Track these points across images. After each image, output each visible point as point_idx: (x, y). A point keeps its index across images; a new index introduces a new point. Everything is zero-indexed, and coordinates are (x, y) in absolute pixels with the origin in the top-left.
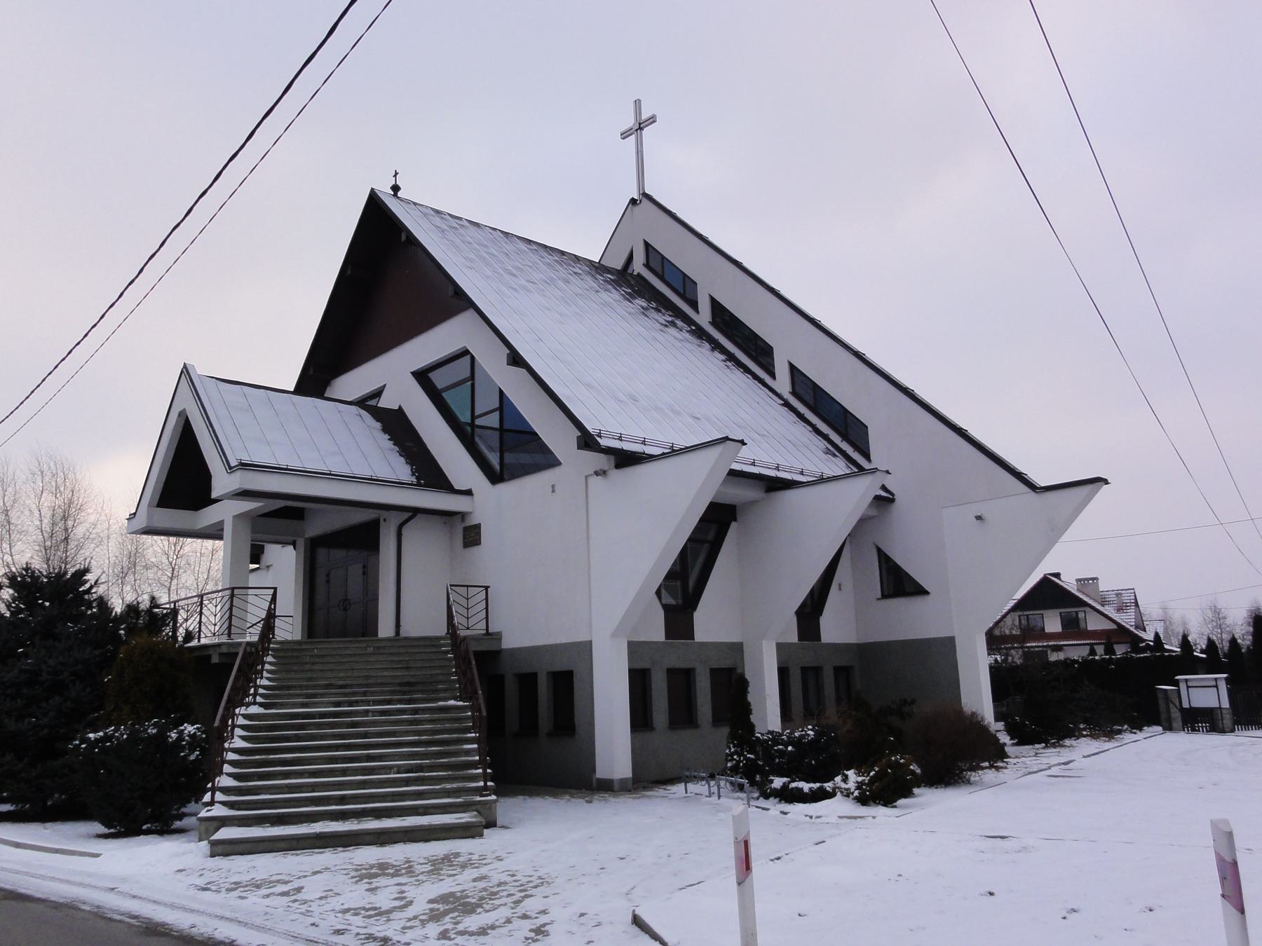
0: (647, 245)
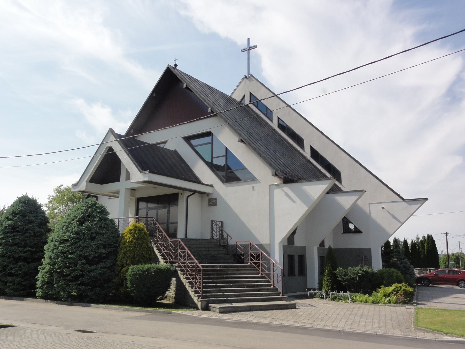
0: (251, 94)
